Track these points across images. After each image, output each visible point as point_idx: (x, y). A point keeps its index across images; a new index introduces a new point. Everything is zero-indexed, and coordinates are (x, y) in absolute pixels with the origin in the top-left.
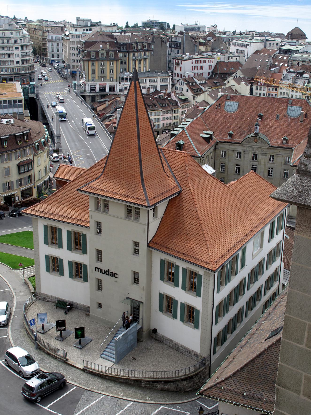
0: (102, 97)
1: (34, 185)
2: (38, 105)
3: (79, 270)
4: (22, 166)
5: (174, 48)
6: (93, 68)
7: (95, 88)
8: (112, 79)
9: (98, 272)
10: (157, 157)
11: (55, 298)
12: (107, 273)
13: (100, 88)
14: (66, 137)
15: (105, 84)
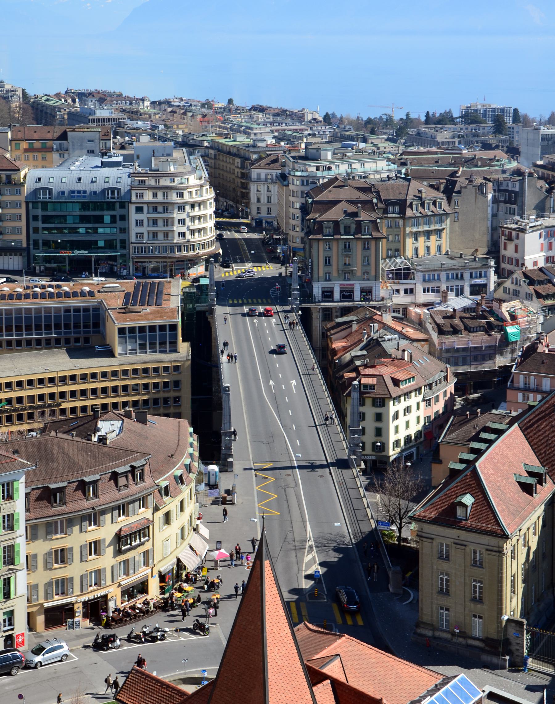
0: (345, 311)
4: (126, 536)
6: (328, 254)
7: (332, 292)
13: (341, 292)
15: (353, 286)
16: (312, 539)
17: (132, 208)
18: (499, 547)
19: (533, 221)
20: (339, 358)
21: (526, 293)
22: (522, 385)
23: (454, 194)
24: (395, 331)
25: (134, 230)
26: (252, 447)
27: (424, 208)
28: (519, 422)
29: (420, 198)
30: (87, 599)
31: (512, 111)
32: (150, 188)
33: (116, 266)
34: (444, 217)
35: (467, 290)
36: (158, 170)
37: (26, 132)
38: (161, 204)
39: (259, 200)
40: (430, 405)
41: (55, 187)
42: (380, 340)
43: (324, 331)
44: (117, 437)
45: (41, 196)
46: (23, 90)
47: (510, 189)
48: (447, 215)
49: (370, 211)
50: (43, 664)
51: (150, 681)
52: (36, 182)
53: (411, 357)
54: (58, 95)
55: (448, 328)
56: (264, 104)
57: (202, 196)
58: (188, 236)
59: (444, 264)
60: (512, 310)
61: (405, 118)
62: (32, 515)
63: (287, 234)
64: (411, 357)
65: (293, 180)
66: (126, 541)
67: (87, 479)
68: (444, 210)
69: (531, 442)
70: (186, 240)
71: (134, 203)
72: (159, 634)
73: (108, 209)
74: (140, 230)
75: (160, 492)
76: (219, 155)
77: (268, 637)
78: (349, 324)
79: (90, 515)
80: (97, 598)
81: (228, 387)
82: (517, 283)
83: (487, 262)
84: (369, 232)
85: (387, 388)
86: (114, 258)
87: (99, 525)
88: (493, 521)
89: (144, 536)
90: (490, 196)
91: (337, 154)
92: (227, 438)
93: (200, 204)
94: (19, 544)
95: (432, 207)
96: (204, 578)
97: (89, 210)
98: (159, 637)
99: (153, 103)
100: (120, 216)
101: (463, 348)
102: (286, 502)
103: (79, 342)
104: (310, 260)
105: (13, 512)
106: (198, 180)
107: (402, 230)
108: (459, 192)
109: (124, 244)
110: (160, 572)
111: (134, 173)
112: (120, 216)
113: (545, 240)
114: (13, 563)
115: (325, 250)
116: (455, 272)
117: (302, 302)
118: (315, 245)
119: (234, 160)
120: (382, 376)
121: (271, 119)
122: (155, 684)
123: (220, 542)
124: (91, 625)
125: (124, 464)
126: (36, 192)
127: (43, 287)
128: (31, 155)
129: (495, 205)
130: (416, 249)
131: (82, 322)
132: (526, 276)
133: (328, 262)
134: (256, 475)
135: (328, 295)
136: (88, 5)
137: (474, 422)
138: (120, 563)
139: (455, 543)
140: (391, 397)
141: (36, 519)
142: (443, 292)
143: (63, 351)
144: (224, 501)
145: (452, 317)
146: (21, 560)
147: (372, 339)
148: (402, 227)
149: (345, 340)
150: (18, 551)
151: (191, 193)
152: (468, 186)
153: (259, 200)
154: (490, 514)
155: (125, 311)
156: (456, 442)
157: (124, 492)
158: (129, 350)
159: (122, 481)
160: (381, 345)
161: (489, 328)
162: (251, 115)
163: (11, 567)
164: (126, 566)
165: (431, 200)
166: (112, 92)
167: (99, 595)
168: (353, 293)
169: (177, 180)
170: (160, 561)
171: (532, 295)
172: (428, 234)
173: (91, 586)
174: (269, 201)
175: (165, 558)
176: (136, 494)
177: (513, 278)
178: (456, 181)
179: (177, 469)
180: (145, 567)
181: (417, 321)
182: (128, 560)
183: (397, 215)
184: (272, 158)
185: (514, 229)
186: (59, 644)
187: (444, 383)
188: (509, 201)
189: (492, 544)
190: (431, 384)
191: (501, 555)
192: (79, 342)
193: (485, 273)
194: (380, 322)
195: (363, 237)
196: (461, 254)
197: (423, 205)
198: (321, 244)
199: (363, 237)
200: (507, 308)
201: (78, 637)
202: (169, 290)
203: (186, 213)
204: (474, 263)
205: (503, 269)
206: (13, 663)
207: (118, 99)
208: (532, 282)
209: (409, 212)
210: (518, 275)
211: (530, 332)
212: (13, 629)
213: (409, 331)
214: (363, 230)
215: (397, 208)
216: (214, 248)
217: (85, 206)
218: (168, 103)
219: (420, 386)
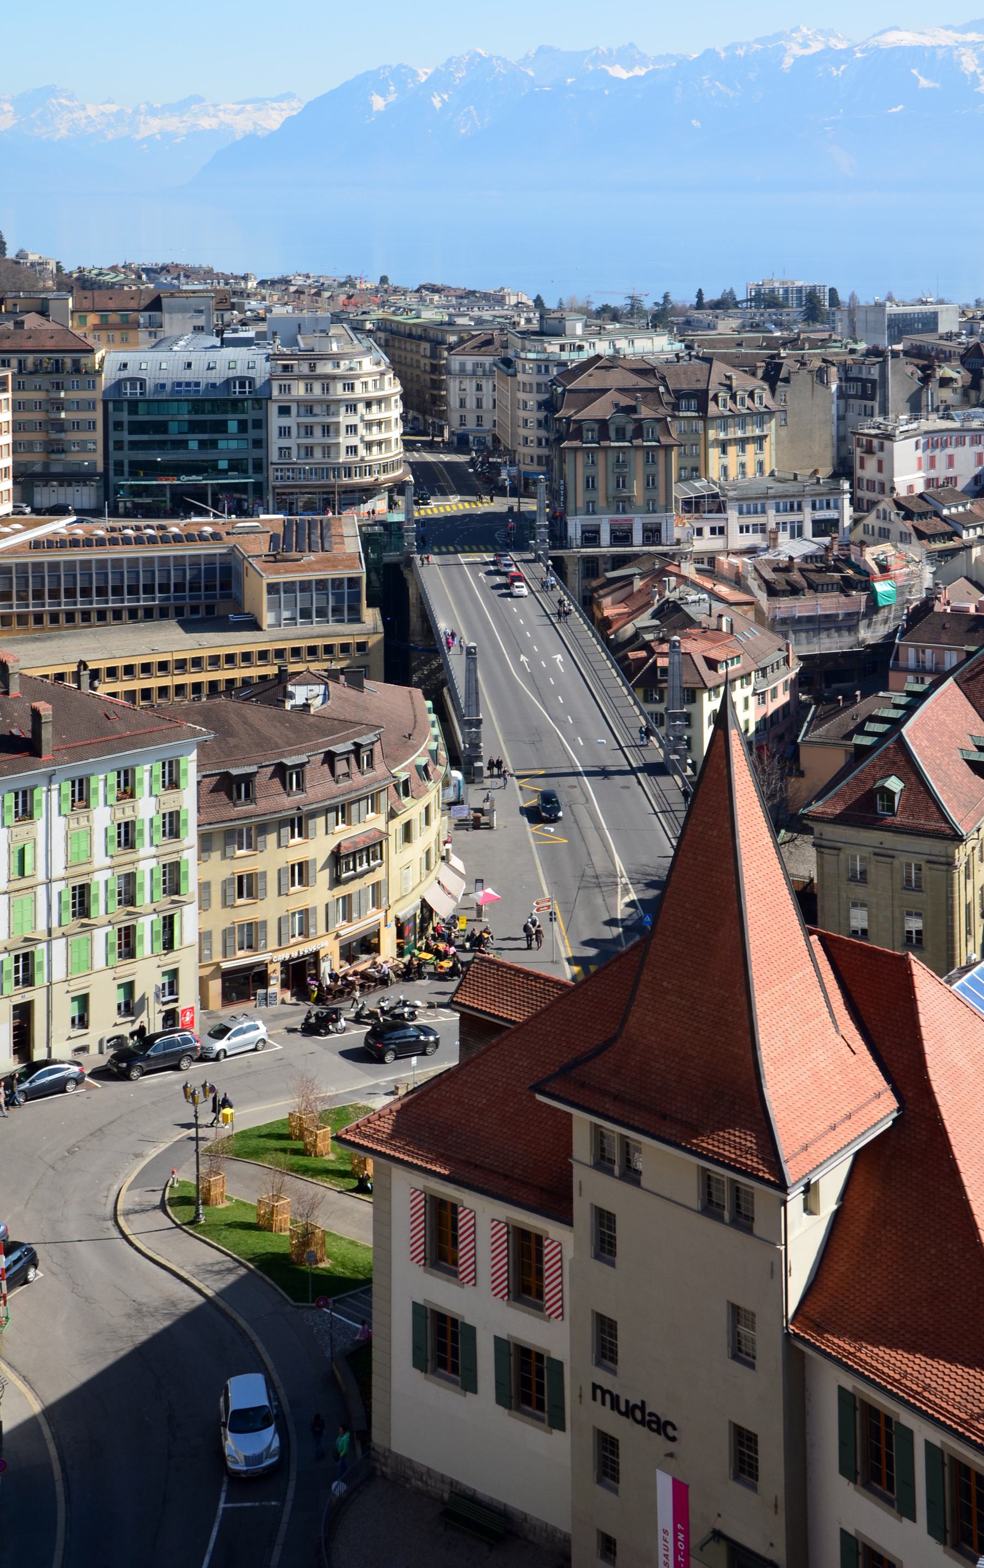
0: (619, 561)
1: (386, 916)
2: (412, 591)
3: (534, 1379)
4: (347, 856)
5: (855, 397)
6: (591, 471)
8: (653, 505)
9: (603, 1403)
10: (810, 981)
11: (443, 1479)
12: (638, 1415)
14: (500, 719)
16: (625, 874)
17: (273, 409)
18: (947, 856)
19: (904, 422)
20: (615, 632)
21: (901, 533)
22: (912, 663)
23: (779, 383)
24: (703, 589)
25: (275, 442)
26: (507, 748)
27: (735, 403)
28: (955, 675)
29: (730, 387)
30: (287, 958)
31: (827, 290)
32: (301, 377)
33: (246, 500)
34: (766, 417)
35: (808, 529)
36: (313, 351)
37: (97, 299)
38: (320, 402)
39: (462, 404)
40: (764, 702)
41: (152, 377)
42: (679, 602)
43: (588, 594)
44: (324, 706)
45: (128, 391)
46: (57, 263)
47: (864, 377)
48: (771, 413)
49: (654, 404)
50: (228, 1054)
51: (506, 973)
52: (120, 370)
53: (732, 626)
54: (114, 269)
55: (782, 586)
56: (438, 282)
57: (383, 390)
58: (362, 451)
59: (771, 488)
60: (882, 557)
61: (661, 302)
62: (205, 818)
63: (515, 451)
64: (732, 626)
65: (524, 366)
66: (347, 864)
67: (288, 762)
68: (766, 407)
69: (977, 705)
70: (358, 459)
71: (276, 401)
72: (406, 1009)
73: (235, 411)
74: (285, 443)
75: (396, 787)
76: (393, 339)
77: (742, 846)
78: (628, 579)
79: (292, 821)
80: (303, 956)
81: (474, 648)
82: (885, 516)
83: (838, 484)
84: (655, 436)
85: (699, 673)
86: (242, 488)
87: (307, 837)
88: (936, 815)
89: (375, 858)
90: (834, 387)
91: (590, 326)
92: (473, 730)
93: (379, 401)
94: (187, 860)
95: (748, 402)
96: (462, 933)
97: (203, 413)
98: (406, 1015)
99: (262, 283)
100: (254, 421)
101: (808, 617)
102: (575, 825)
103: (198, 613)
104: (562, 482)
105: (178, 808)
106: (375, 367)
107: (702, 436)
108: (787, 380)
109: (259, 466)
110: (397, 920)
111: (275, 355)
112: (254, 421)
113: (924, 451)
114: (177, 892)
115: (586, 465)
116: (788, 500)
117: (552, 548)
118: (569, 457)
119: (418, 346)
120: (689, 654)
121: (454, 301)
122: (514, 975)
123: (482, 881)
124: (294, 1000)
125: (344, 740)
126: (118, 385)
127: (138, 528)
128: (103, 334)
129: (842, 402)
130: (725, 468)
131: (203, 581)
132: (898, 505)
133: (590, 484)
134: (521, 788)
135: (591, 537)
136: (145, 146)
137: (852, 710)
138: (338, 899)
139: (875, 854)
140: (706, 687)
141: (210, 824)
142: (770, 532)
143: (174, 622)
144: (477, 825)
145: (787, 569)
146: (190, 886)
147: (667, 601)
148: (701, 432)
149: (623, 605)
150: (186, 873)
151: (365, 383)
152: (801, 371)
153: (462, 404)
154: (931, 804)
155: (275, 558)
156: (825, 741)
157: (345, 784)
158: (285, 619)
159: (341, 767)
160: (682, 610)
161: (846, 586)
162: (421, 297)
163: (176, 897)
164: (347, 907)
165: (746, 391)
166: (197, 266)
167: (306, 952)
168: (631, 533)
169: (344, 364)
170: (397, 901)
171: (910, 534)
172: (742, 442)
173: (293, 936)
174: (479, 404)
175: (404, 896)
176: (362, 789)
177: (878, 510)
178: (781, 364)
179: (419, 756)
180: (374, 909)
181: (733, 578)
182: (350, 896)
183: (694, 414)
184: (483, 338)
185: (876, 436)
186: (252, 1023)
187: (783, 668)
188: (864, 396)
189: (935, 852)
190: (765, 668)
191: (951, 868)
192: (198, 613)
193: (836, 501)
194: (678, 576)
195: (645, 444)
196: (795, 475)
197: (733, 397)
198: (580, 457)
199: (645, 444)
200: (873, 554)
201: (276, 1017)
202: (340, 530)
203: (359, 415)
204: (817, 487)
205: (860, 500)
206: (184, 1051)
207: (206, 276)
208: (909, 515)
209: (712, 409)
210: (886, 504)
211: (910, 592)
212: (176, 1001)
213: (723, 590)
214: (645, 434)
215: (693, 403)
216: (401, 471)
217: (197, 405)
218: (286, 282)
219: (748, 670)
